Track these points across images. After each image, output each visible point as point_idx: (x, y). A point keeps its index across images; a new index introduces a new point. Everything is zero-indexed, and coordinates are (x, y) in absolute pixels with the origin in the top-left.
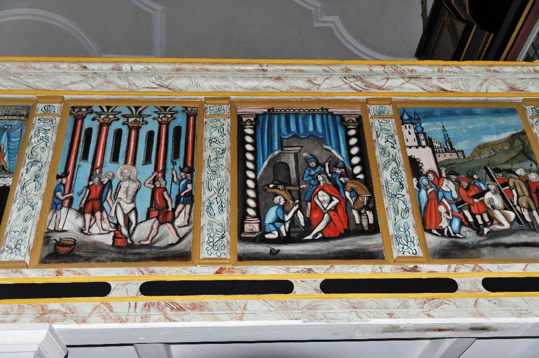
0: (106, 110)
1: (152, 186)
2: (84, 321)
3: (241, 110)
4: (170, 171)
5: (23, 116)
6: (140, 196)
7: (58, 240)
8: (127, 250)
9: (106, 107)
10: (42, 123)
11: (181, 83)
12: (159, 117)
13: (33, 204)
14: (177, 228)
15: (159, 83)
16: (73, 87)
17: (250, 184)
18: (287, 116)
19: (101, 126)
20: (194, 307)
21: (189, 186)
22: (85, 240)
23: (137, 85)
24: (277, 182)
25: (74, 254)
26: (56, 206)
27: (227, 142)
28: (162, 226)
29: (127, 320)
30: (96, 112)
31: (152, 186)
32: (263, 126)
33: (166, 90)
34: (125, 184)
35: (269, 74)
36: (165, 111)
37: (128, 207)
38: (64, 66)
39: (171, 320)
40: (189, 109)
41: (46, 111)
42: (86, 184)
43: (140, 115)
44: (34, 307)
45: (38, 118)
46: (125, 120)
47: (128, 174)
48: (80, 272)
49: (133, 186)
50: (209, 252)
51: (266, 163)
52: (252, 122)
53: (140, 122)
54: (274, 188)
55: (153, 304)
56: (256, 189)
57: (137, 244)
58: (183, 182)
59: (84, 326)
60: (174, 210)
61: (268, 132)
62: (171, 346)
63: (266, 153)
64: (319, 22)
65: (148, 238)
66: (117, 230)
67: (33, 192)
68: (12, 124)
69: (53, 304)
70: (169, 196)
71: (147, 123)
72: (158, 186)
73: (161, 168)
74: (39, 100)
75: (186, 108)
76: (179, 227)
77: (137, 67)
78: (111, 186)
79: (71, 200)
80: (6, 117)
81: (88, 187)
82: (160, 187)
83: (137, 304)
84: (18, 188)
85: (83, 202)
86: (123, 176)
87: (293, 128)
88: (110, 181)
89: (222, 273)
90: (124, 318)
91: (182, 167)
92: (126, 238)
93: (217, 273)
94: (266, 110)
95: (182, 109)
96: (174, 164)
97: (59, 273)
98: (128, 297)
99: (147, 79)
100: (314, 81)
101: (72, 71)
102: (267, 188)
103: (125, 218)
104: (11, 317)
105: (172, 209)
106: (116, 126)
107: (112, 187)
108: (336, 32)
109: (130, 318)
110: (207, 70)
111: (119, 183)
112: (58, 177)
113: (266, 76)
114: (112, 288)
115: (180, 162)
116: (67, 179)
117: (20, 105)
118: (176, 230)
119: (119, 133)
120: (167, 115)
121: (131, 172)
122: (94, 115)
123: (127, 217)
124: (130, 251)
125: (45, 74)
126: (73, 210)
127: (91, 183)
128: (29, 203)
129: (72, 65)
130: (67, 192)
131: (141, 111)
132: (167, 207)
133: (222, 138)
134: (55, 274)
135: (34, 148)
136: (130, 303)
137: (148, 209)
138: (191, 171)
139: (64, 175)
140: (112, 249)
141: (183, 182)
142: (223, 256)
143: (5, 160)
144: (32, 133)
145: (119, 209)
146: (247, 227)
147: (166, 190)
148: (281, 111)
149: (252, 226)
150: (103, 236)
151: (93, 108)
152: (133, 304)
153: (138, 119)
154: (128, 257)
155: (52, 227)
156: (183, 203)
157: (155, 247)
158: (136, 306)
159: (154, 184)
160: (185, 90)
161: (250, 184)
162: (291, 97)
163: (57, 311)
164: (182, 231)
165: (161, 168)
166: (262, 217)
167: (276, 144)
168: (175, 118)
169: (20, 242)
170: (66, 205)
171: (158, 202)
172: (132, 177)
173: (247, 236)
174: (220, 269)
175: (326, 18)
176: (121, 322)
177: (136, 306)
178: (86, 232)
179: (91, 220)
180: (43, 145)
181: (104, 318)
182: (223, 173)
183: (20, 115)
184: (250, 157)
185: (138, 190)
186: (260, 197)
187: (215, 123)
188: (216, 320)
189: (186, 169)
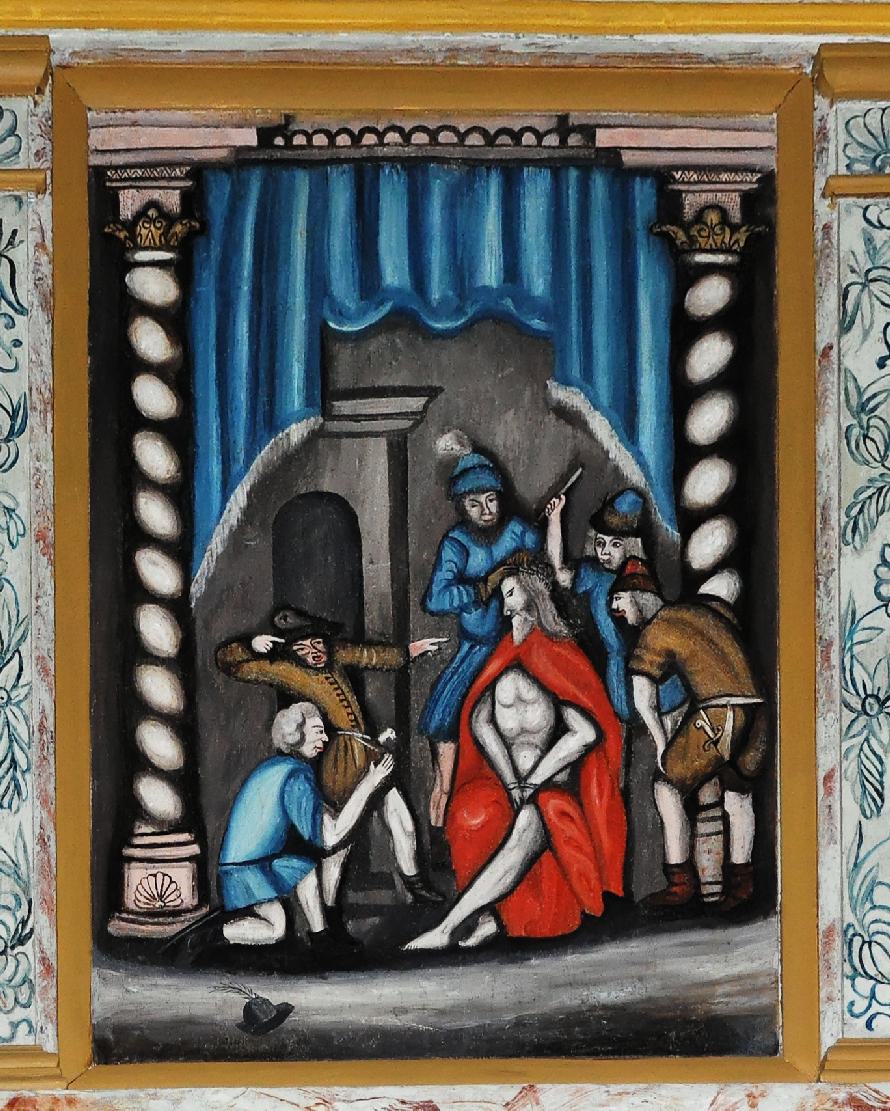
18: (366, 174)
24: (292, 621)
51: (240, 497)
54: (275, 655)
56: (183, 665)
87: (394, 271)
94: (250, 137)
142: (23, 1038)
146: (139, 883)
166: (211, 826)
186: (205, 710)
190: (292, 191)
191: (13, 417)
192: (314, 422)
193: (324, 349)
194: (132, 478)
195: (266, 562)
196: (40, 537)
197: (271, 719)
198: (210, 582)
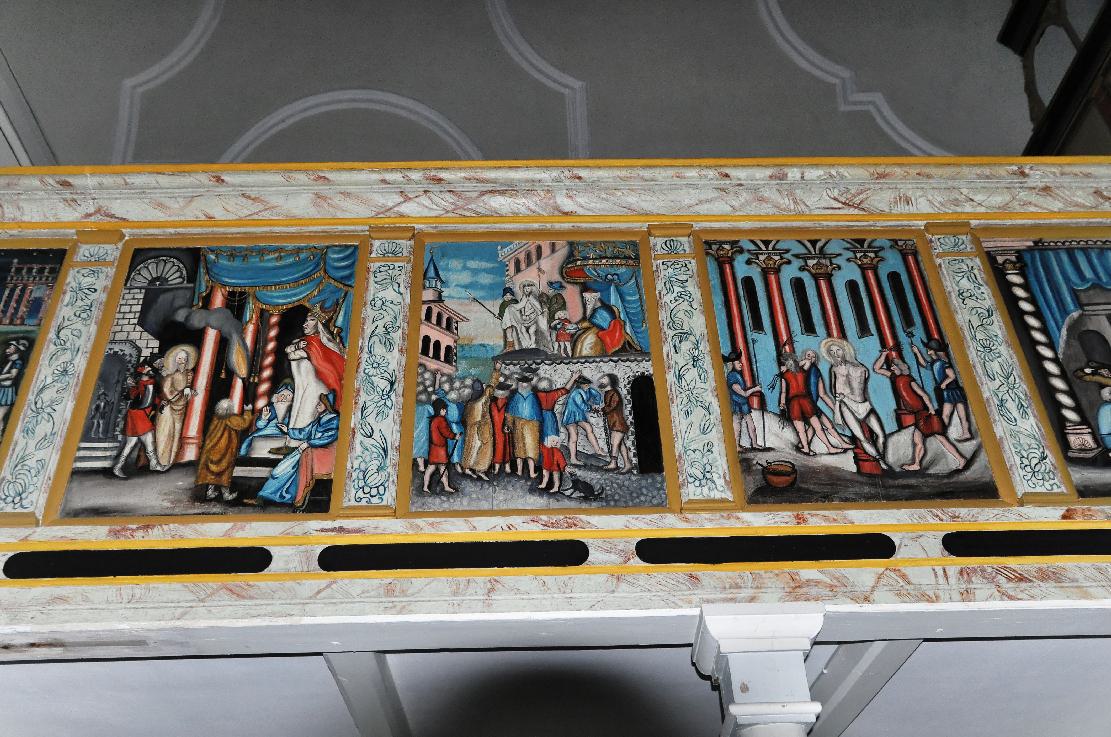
1: (889, 374)
2: (867, 599)
3: (988, 245)
5: (630, 258)
7: (765, 464)
9: (809, 241)
11: (881, 199)
12: (856, 258)
14: (955, 443)
16: (703, 209)
17: (1051, 367)
18: (1070, 252)
19: (765, 273)
20: (1044, 576)
21: (949, 372)
22: (811, 464)
26: (741, 409)
27: (987, 297)
28: (928, 440)
29: (938, 598)
30: (749, 251)
31: (889, 374)
32: (1036, 269)
33: (856, 211)
34: (841, 370)
35: (1030, 182)
36: (862, 246)
37: (862, 410)
38: (692, 173)
39: (1011, 598)
40: (900, 243)
43: (822, 253)
44: (777, 575)
46: (800, 262)
47: (840, 352)
49: (857, 374)
51: (1064, 332)
54: (1093, 374)
55: (974, 570)
56: (1063, 376)
58: (937, 366)
59: (867, 608)
60: (939, 412)
61: (1048, 280)
63: (1058, 317)
64: (846, 102)
66: (857, 447)
67: (700, 384)
69: (808, 570)
70: (923, 389)
71: (839, 268)
72: (897, 372)
74: (378, 231)
75: (895, 241)
76: (959, 441)
77: (813, 174)
78: (819, 375)
81: (781, 375)
82: (901, 375)
85: (783, 401)
86: (833, 357)
87: (1088, 274)
88: (814, 365)
89: (1073, 518)
90: (931, 593)
91: (926, 341)
92: (878, 461)
93: (1064, 517)
94: (1031, 244)
95: (888, 244)
96: (910, 335)
97: (800, 519)
98: (928, 559)
99: (825, 194)
100: (1105, 193)
102: (1082, 374)
103: (861, 427)
104: (746, 593)
105: (936, 411)
106: (789, 273)
107: (821, 375)
108: (879, 120)
109: (941, 593)
110: (929, 176)
111: (830, 369)
112: (726, 359)
113: (1026, 185)
115: (919, 332)
116: (741, 362)
118: (954, 446)
119: (798, 286)
122: (746, 256)
124: (891, 482)
125: (657, 188)
127: (784, 369)
129: (703, 172)
131: (822, 247)
133: (980, 292)
134: (795, 521)
135: (674, 312)
137: (895, 411)
138: (943, 346)
140: (860, 478)
141: (937, 366)
142: (1056, 490)
143: (628, 331)
144: (660, 286)
145: (844, 409)
147: (914, 380)
149: (1080, 439)
151: (740, 244)
152: (940, 572)
153: (823, 261)
154: (892, 492)
156: (950, 401)
157: (930, 475)
159: (889, 369)
160: (887, 211)
161: (1051, 367)
162: (1069, 221)
163: (817, 583)
164: (968, 448)
165: (891, 343)
167: (1069, 299)
169: (708, 468)
170: (755, 406)
174: (1067, 511)
175: (862, 97)
178: (806, 450)
179: (806, 431)
180: (685, 306)
181: (898, 595)
182: (1003, 349)
184: (1032, 322)
185: (866, 380)
187: (957, 266)
189: (933, 344)
190: (1049, 259)
191: (988, 311)
193: (1076, 294)
196: (1007, 342)
197: (1100, 394)
198: (1064, 354)
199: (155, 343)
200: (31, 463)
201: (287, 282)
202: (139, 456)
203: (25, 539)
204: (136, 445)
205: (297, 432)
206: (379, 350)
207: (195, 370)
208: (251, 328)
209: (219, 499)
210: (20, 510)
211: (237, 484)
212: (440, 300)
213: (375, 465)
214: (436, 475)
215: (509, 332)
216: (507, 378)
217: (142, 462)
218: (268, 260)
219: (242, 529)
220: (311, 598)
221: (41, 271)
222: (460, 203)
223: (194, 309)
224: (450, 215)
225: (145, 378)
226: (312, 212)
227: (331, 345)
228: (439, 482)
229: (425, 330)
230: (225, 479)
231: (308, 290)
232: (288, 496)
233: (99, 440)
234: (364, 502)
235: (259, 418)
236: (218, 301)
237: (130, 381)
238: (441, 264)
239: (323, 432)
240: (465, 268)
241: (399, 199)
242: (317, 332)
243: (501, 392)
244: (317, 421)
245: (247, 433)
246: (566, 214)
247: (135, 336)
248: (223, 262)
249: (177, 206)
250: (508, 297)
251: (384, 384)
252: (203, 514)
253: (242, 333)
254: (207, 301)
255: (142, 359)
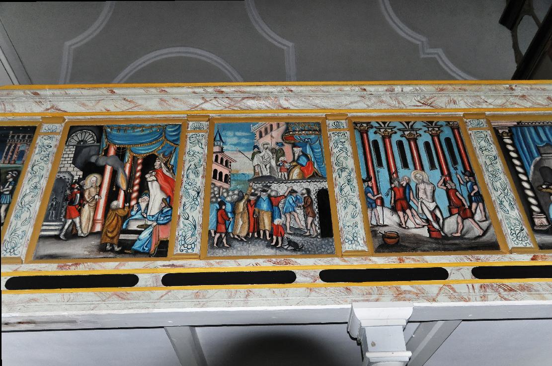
0: (383, 125)
1: (445, 188)
2: (434, 300)
4: (455, 175)
5: (317, 130)
6: (438, 197)
8: (443, 241)
9: (405, 122)
10: (336, 137)
11: (441, 102)
13: (355, 203)
15: (423, 102)
16: (353, 106)
17: (526, 185)
18: (535, 128)
19: (384, 138)
20: (522, 288)
21: (475, 187)
23: (405, 104)
24: (547, 183)
25: (401, 245)
26: (371, 205)
27: (494, 150)
28: (465, 221)
29: (469, 300)
31: (445, 188)
32: (518, 136)
33: (429, 107)
34: (422, 186)
35: (515, 93)
37: (432, 206)
38: (347, 89)
39: (506, 299)
40: (451, 123)
41: (337, 127)
42: (390, 187)
43: (412, 128)
45: (332, 132)
48: (419, 259)
49: (429, 189)
50: (515, 242)
51: (532, 167)
52: (508, 133)
53: (415, 135)
54: (547, 188)
55: (488, 286)
56: (532, 189)
57: (450, 236)
58: (469, 184)
59: (435, 304)
60: (470, 207)
62: (196, 328)
65: (457, 230)
66: (429, 225)
68: (311, 138)
70: (462, 196)
71: (420, 135)
72: (449, 187)
73: (446, 173)
75: (449, 122)
76: (480, 222)
77: (407, 89)
78: (410, 189)
79: (382, 199)
80: (304, 132)
81: (392, 189)
82: (451, 189)
83: (474, 286)
84: (337, 190)
85: (393, 202)
86: (418, 180)
87: (544, 138)
88: (408, 184)
89: (537, 260)
93: (532, 259)
94: (516, 124)
95: (445, 123)
96: (456, 169)
97: (401, 260)
101: (353, 93)
102: (541, 188)
103: (431, 214)
104: (374, 297)
105: (469, 206)
106: (396, 138)
107: (411, 189)
109: (471, 297)
113: (513, 94)
114: (449, 272)
115: (460, 167)
117: (312, 122)
120: (435, 129)
121: (423, 176)
122: (374, 130)
123: (432, 213)
124: (446, 242)
126: (387, 208)
127: (393, 186)
128: (351, 203)
129: (353, 88)
130: (376, 193)
132: (464, 205)
133: (490, 147)
136: (468, 285)
137: (448, 206)
138: (472, 174)
139: (368, 179)
140: (431, 240)
141: (469, 184)
142: (528, 246)
143: (316, 167)
144: (331, 144)
145: (423, 205)
146: (537, 221)
147: (458, 191)
148: (543, 123)
150: (419, 229)
151: (372, 124)
152: (471, 287)
153: (412, 132)
155: (374, 223)
156: (475, 202)
157: (465, 239)
158: (473, 287)
159: (445, 186)
161: (526, 185)
163: (410, 292)
164: (485, 225)
165: (446, 173)
166: (546, 213)
168: (442, 131)
169: (355, 235)
170: (379, 204)
171: (454, 200)
172: (425, 180)
173: (538, 228)
174: (534, 256)
175: (432, 51)
176: (464, 301)
177: (473, 287)
178: (404, 226)
179: (404, 217)
180: (344, 154)
182: (502, 176)
183: (314, 130)
184: (517, 162)
185: (434, 191)
186: (538, 196)
187: (479, 135)
188: (543, 298)
189: (467, 173)
192: (540, 157)
194: (514, 165)
195: (540, 175)
198: (532, 178)
199: (81, 173)
200: (19, 232)
201: (146, 143)
202: (72, 229)
203: (16, 270)
204: (71, 223)
205: (151, 217)
206: (192, 176)
207: (101, 186)
208: (128, 165)
209: (112, 250)
210: (13, 256)
211: (121, 243)
212: (222, 151)
213: (189, 234)
214: (220, 238)
215: (256, 167)
216: (255, 190)
217: (74, 232)
218: (137, 132)
219: (124, 265)
220: (158, 299)
221: (24, 137)
222: (232, 103)
223: (100, 155)
224: (227, 109)
225: (76, 190)
226: (159, 108)
227: (168, 174)
228: (222, 242)
229: (215, 166)
230: (115, 241)
231: (156, 146)
232: (147, 249)
233: (53, 221)
234: (184, 252)
235: (132, 210)
236: (112, 152)
237: (68, 192)
238: (223, 134)
239: (164, 217)
240: (235, 136)
241: (201, 101)
242: (161, 167)
243: (252, 197)
244: (161, 211)
245: (126, 218)
246: (285, 109)
247: (70, 169)
248: (114, 132)
249: (91, 105)
250: (256, 150)
251: (194, 193)
252: (104, 258)
253: (124, 167)
254: (106, 152)
255: (74, 181)
